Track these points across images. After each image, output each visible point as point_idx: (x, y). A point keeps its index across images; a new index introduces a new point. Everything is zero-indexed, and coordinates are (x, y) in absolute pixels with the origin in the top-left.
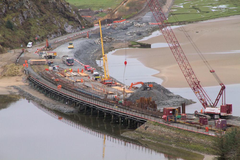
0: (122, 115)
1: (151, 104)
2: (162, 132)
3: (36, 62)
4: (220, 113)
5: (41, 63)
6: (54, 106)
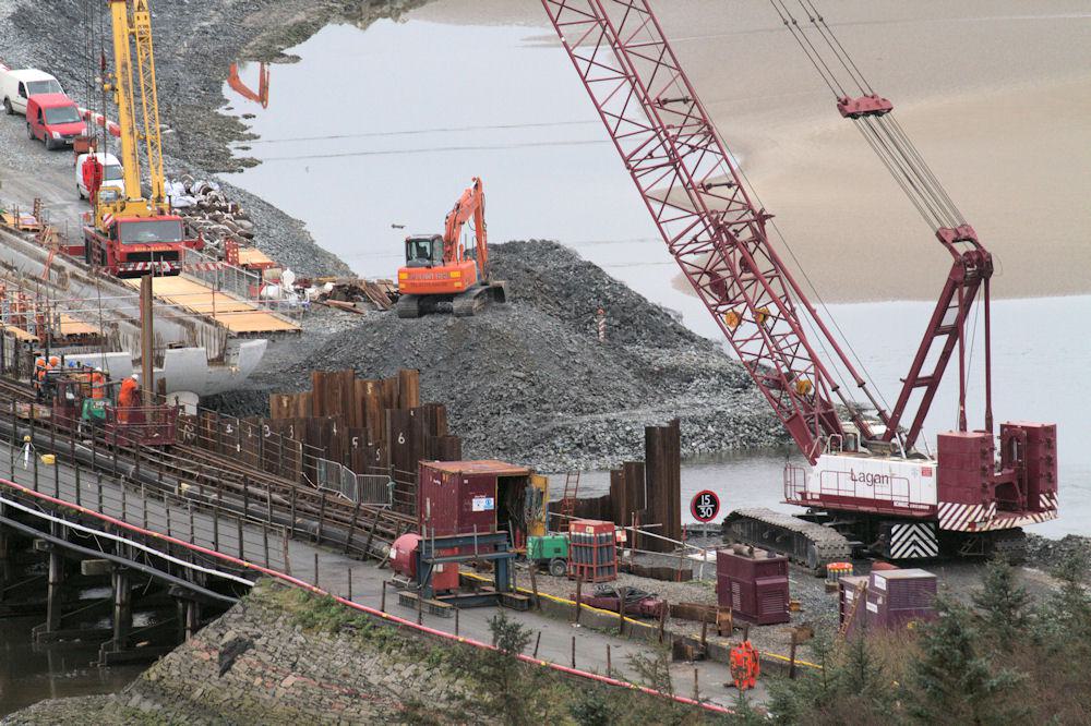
0: (71, 529)
1: (401, 440)
2: (357, 696)
4: (934, 508)
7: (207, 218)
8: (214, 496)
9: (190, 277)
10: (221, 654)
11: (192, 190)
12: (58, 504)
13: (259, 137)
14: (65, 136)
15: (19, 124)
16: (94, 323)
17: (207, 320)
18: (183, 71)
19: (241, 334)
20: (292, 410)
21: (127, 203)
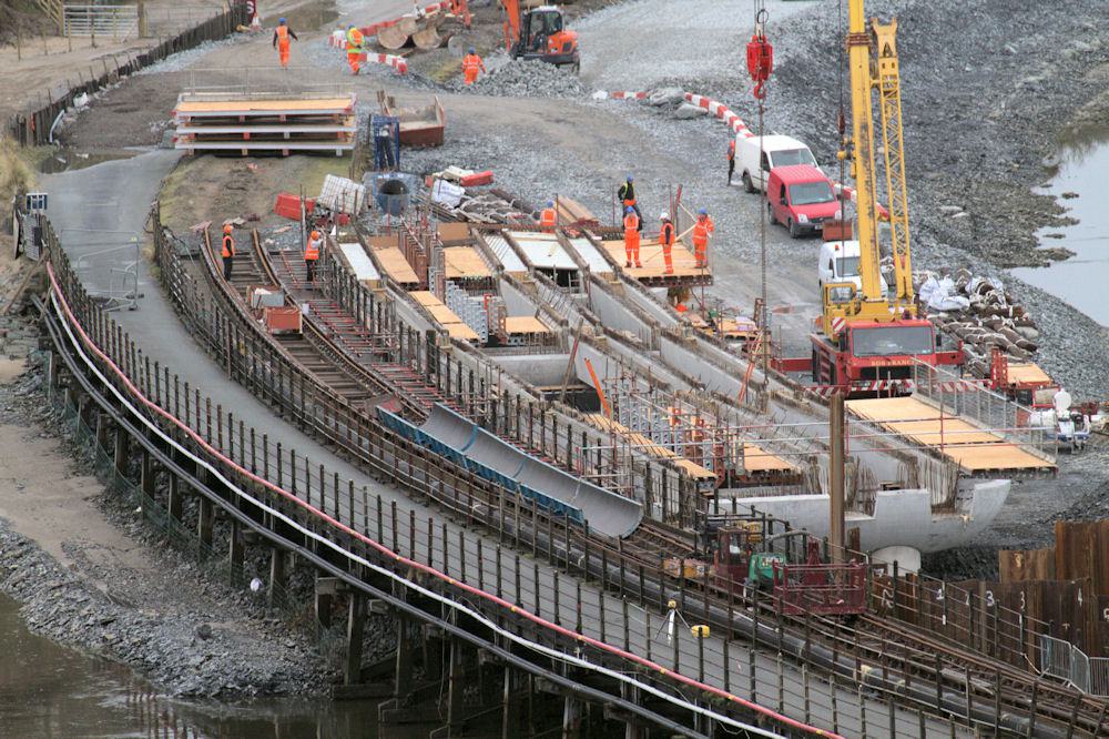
3: (234, 120)
5: (295, 137)
6: (105, 624)
7: (980, 324)
8: (901, 682)
9: (923, 398)
11: (967, 289)
12: (702, 690)
13: (1078, 222)
14: (814, 220)
15: (754, 204)
16: (788, 457)
17: (935, 454)
18: (993, 138)
19: (978, 473)
20: (1028, 572)
21: (863, 304)
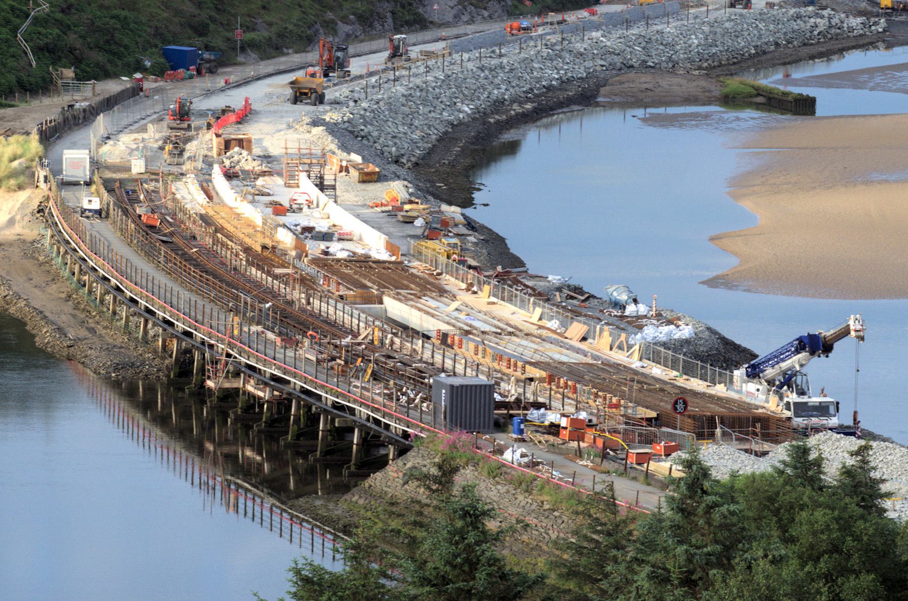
10: (405, 474)
